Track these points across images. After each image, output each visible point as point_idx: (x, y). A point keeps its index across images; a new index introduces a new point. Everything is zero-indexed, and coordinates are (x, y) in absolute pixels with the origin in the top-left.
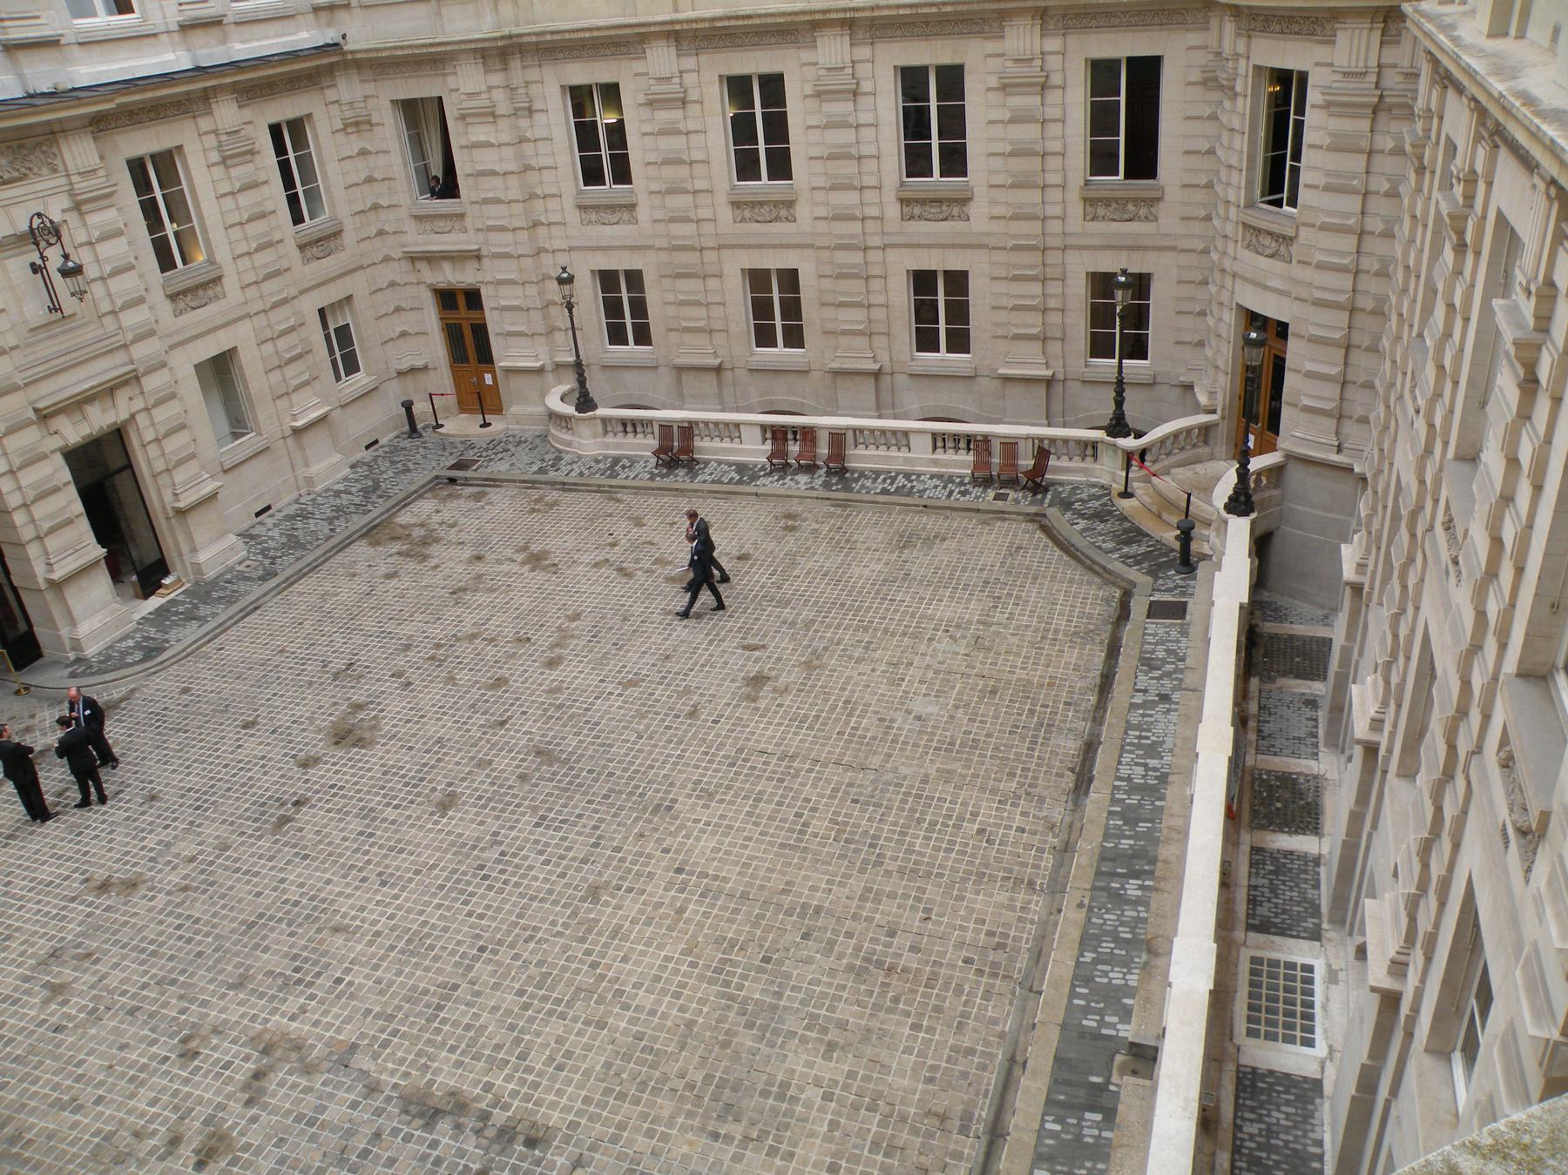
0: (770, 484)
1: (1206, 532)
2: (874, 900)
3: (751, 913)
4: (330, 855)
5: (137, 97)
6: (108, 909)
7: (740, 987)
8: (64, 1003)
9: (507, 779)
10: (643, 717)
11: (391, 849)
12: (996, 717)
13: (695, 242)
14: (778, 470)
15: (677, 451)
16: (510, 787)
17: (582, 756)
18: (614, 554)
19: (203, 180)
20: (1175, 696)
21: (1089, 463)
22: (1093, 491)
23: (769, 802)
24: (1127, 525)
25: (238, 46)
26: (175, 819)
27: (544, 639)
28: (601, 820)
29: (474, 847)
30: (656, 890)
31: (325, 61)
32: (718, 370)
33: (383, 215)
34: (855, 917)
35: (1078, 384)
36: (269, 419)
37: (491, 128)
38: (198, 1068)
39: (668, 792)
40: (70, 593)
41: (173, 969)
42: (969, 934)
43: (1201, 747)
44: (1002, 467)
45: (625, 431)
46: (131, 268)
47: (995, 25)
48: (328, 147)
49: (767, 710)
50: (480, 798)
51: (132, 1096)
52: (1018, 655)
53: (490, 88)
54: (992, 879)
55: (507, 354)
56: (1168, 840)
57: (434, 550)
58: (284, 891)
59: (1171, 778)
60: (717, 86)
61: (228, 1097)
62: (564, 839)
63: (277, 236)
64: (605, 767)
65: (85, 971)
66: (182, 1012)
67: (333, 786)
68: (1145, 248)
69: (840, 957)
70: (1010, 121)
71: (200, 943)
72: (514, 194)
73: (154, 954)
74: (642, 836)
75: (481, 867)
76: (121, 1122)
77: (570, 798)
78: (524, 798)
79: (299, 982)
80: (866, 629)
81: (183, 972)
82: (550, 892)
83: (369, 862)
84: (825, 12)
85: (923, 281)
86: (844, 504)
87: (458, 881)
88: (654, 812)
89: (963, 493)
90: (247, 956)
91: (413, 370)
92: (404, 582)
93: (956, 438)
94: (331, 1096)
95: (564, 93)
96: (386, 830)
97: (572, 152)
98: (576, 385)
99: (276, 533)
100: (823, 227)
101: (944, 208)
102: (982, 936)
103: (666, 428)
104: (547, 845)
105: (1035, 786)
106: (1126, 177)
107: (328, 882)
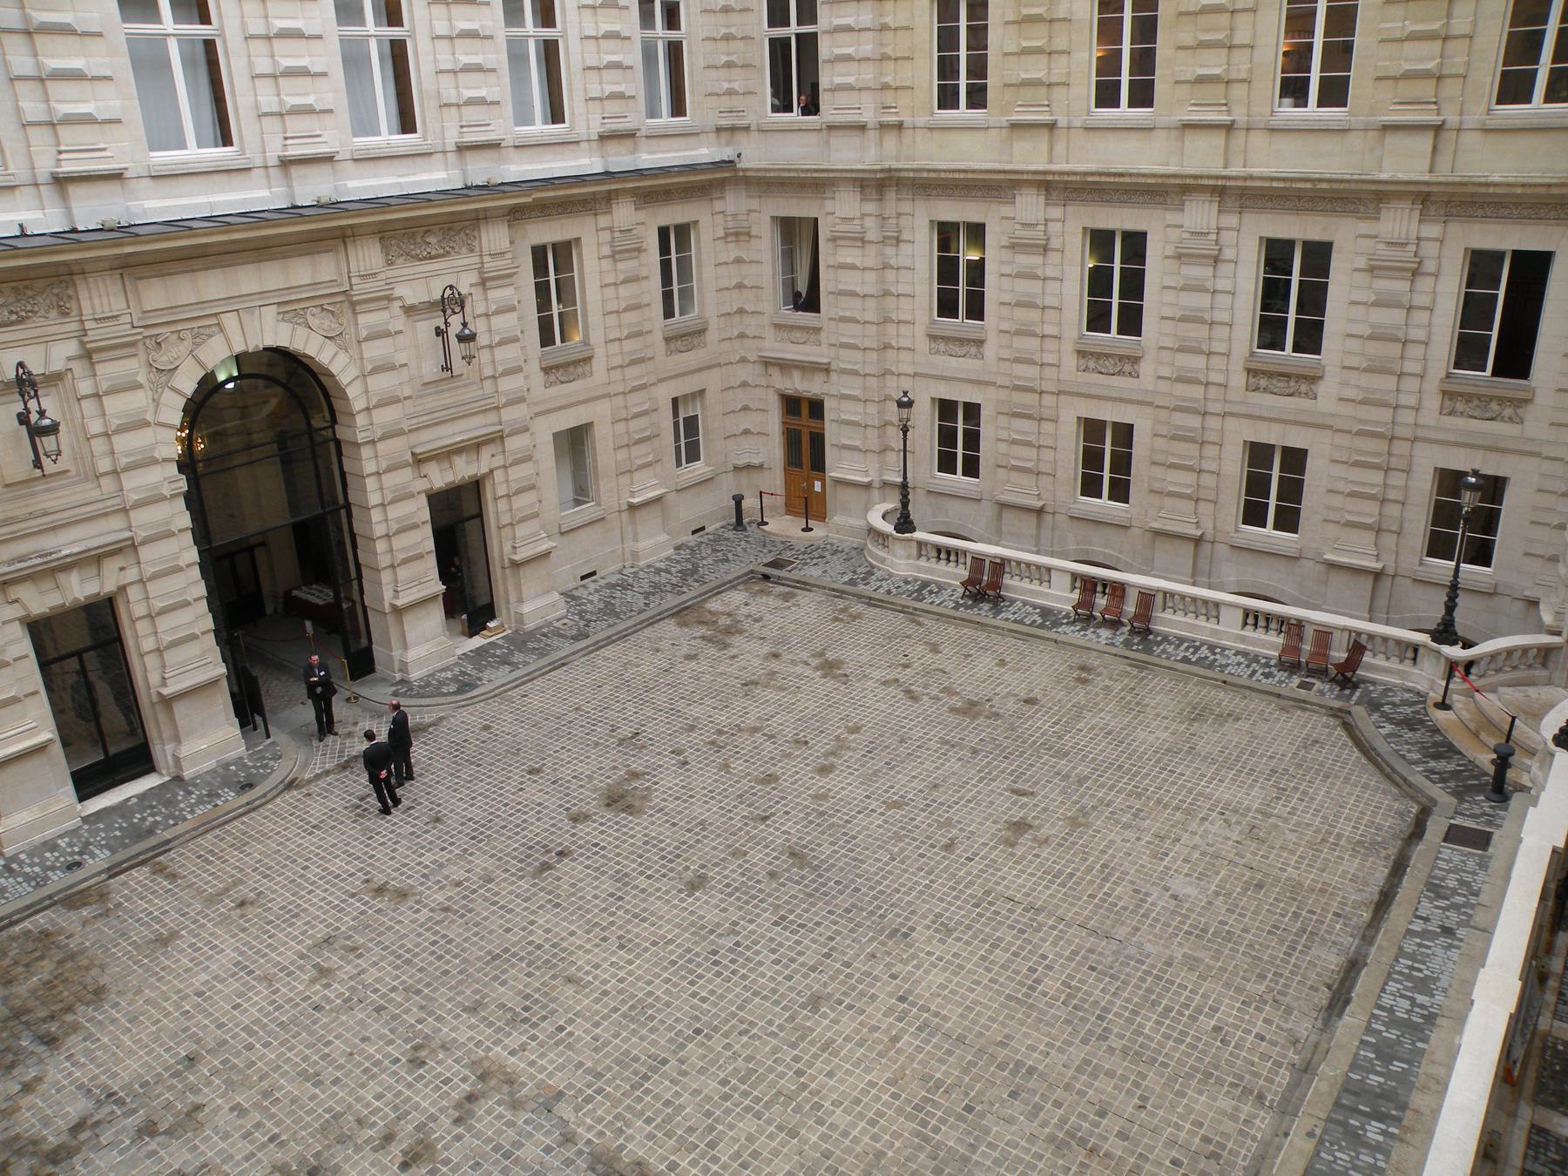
0: (1070, 633)
1: (1528, 762)
2: (1091, 1074)
3: (964, 1058)
4: (579, 908)
5: (552, 194)
6: (379, 911)
7: (936, 1130)
8: (327, 986)
9: (757, 873)
10: (900, 839)
11: (636, 916)
12: (1257, 913)
13: (1036, 385)
14: (1081, 621)
15: (985, 585)
16: (758, 882)
17: (833, 866)
18: (905, 676)
19: (593, 271)
20: (1461, 932)
21: (1407, 666)
22: (1407, 696)
23: (1006, 950)
24: (1438, 738)
25: (645, 156)
26: (452, 844)
27: (820, 745)
28: (838, 933)
29: (711, 932)
30: (875, 1013)
31: (718, 176)
32: (1040, 512)
33: (747, 319)
34: (1068, 1087)
35: (1408, 581)
36: (610, 492)
37: (858, 252)
38: (422, 1077)
39: (908, 919)
40: (408, 620)
41: (420, 980)
42: (1183, 1134)
43: (1478, 993)
44: (1313, 655)
45: (939, 558)
46: (516, 340)
47: (1371, 206)
48: (707, 251)
49: (1023, 857)
50: (728, 885)
51: (363, 1086)
52: (1293, 852)
53: (864, 215)
54: (1220, 1082)
55: (839, 466)
56: (1424, 1089)
57: (736, 640)
58: (531, 933)
59: (1439, 1021)
60: (1075, 427)
61: (441, 1110)
62: (798, 943)
63: (647, 327)
64: (853, 881)
65: (349, 962)
66: (420, 1021)
67: (596, 845)
68: (1504, 451)
69: (1044, 1124)
70: (1374, 304)
71: (448, 962)
72: (871, 316)
73: (408, 962)
74: (874, 956)
75: (715, 953)
76: (350, 1107)
77: (813, 905)
78: (769, 895)
79: (525, 1020)
80: (1139, 796)
81: (428, 985)
82: (774, 991)
83: (612, 924)
84: (1196, 177)
85: (1259, 454)
86: (1142, 666)
87: (690, 961)
88: (890, 936)
89: (1267, 676)
90: (486, 985)
91: (749, 467)
92: (702, 665)
93: (1268, 617)
94: (530, 1135)
95: (932, 228)
96: (634, 897)
97: (931, 284)
98: (899, 505)
99: (595, 598)
100: (1164, 386)
101: (1292, 383)
102: (1197, 1140)
103: (978, 561)
104: (781, 945)
105: (1284, 994)
106: (1494, 374)
107: (572, 934)
